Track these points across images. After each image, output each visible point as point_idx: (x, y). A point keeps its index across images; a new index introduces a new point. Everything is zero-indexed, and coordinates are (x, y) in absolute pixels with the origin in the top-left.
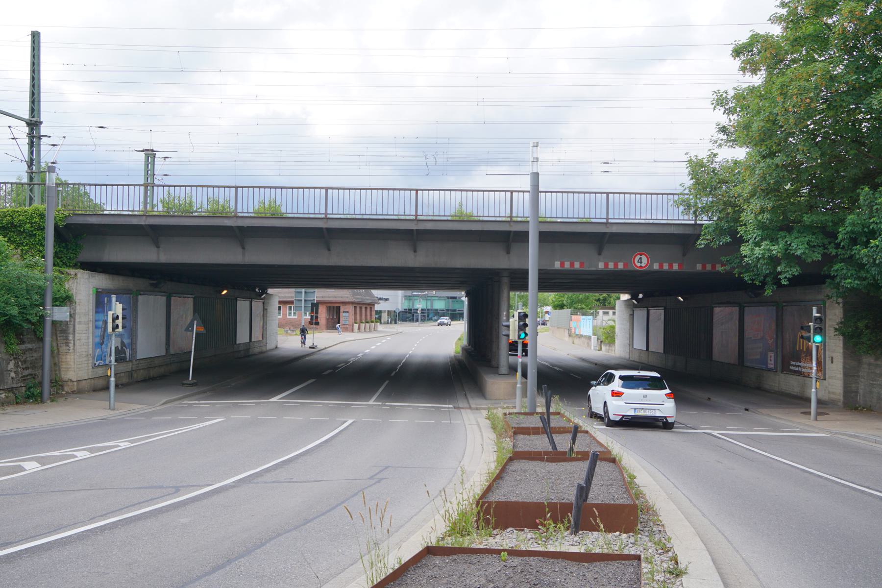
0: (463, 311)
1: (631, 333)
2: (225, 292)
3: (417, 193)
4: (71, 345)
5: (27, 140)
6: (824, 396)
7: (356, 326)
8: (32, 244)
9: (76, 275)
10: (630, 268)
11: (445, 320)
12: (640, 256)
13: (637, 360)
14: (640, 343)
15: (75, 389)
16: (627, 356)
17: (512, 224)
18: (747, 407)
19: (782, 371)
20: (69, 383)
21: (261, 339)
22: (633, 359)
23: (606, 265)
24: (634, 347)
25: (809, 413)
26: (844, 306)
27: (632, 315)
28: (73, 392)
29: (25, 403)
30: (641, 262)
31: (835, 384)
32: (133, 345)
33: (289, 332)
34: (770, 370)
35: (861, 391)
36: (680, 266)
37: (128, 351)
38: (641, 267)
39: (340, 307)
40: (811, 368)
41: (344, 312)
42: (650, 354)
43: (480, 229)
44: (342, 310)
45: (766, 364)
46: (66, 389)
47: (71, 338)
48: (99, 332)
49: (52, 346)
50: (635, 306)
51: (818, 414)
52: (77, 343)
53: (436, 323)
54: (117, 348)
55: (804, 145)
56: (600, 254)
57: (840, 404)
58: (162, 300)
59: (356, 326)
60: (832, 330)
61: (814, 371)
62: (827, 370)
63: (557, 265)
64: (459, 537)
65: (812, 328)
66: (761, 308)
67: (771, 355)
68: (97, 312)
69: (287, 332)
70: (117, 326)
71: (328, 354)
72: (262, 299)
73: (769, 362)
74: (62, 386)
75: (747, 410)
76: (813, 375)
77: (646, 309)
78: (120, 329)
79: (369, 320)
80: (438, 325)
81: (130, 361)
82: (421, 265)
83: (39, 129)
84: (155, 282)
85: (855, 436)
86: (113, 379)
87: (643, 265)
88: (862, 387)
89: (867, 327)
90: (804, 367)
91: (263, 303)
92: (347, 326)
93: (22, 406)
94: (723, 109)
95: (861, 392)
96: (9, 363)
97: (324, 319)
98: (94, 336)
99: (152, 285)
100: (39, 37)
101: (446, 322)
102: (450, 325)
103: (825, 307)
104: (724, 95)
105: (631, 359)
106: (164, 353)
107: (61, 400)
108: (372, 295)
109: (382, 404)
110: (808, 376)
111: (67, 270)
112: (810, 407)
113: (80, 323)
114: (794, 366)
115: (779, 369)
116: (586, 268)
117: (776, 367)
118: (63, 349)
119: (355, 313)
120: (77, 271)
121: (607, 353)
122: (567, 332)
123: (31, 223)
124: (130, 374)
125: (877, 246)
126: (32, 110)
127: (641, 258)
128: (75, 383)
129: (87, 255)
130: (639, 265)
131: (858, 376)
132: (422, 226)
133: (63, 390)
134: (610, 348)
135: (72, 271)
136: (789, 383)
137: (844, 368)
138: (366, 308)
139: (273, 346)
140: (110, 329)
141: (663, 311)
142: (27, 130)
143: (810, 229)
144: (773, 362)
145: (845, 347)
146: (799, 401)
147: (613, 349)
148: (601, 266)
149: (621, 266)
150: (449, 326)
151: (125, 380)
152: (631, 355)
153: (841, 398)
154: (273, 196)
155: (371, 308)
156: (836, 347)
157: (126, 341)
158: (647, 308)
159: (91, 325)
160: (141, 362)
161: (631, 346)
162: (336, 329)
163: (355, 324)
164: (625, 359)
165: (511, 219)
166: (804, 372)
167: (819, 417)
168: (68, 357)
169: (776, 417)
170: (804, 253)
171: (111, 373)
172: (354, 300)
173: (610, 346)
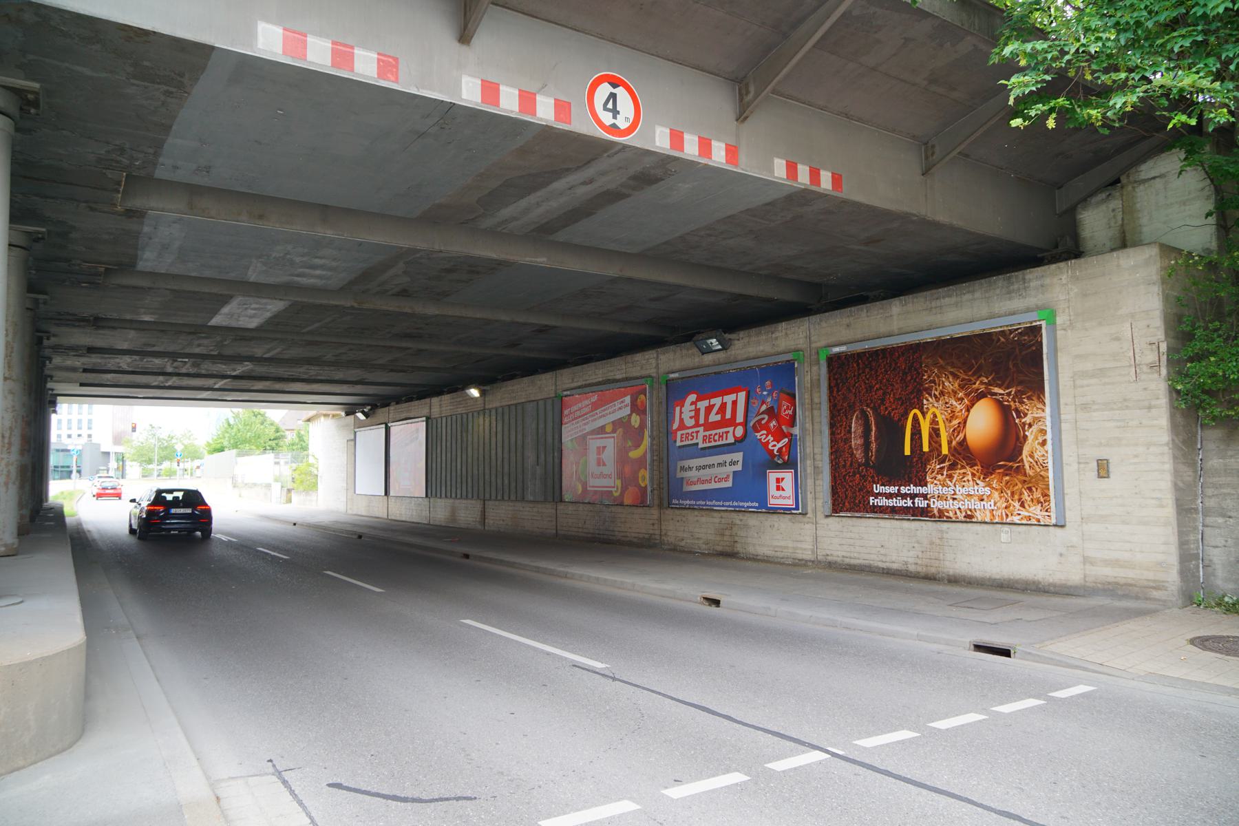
0: (68, 467)
12: (611, 89)
13: (364, 514)
14: (370, 482)
22: (354, 513)
24: (357, 493)
30: (615, 113)
35: (1216, 551)
38: (613, 129)
42: (392, 501)
56: (464, 37)
77: (384, 426)
87: (623, 124)
109: (1031, 323)
116: (406, 83)
122: (230, 482)
127: (613, 96)
130: (607, 118)
152: (349, 507)
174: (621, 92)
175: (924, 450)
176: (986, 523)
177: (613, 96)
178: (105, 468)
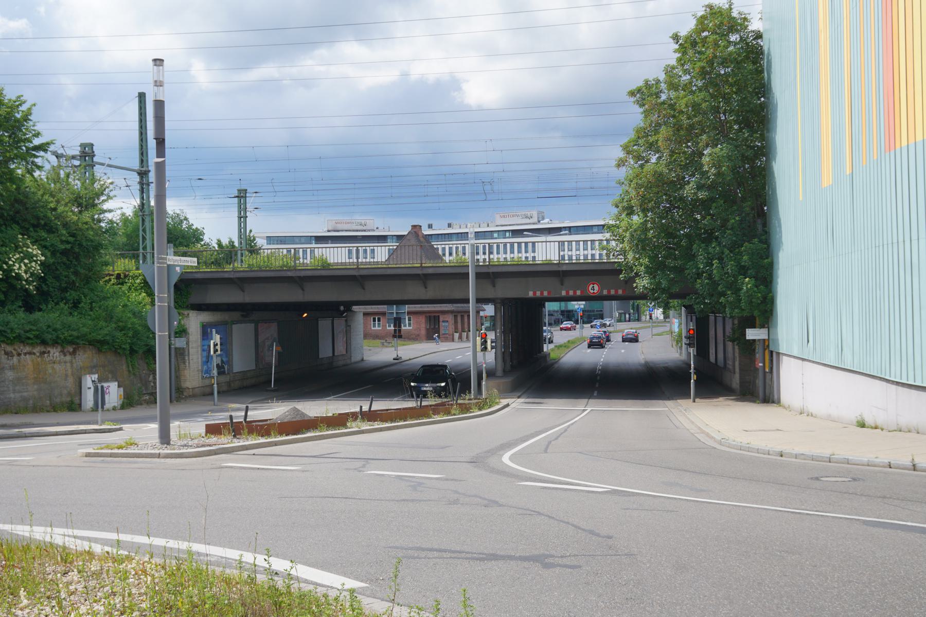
2: (305, 315)
4: (187, 364)
5: (138, 187)
9: (188, 314)
15: (191, 394)
20: (187, 390)
21: (344, 353)
28: (190, 396)
30: (594, 290)
32: (230, 363)
33: (385, 344)
36: (623, 291)
37: (226, 367)
39: (439, 316)
41: (443, 322)
44: (441, 319)
46: (185, 394)
47: (187, 359)
48: (205, 354)
49: (175, 365)
52: (191, 361)
54: (218, 365)
58: (251, 326)
59: (457, 335)
63: (531, 294)
64: (30, 277)
68: (203, 339)
69: (383, 344)
70: (217, 350)
71: (408, 365)
72: (344, 317)
74: (182, 392)
78: (219, 352)
81: (228, 373)
83: (148, 177)
84: (244, 313)
86: (215, 386)
87: (595, 291)
91: (346, 321)
92: (447, 336)
96: (149, 377)
97: (424, 329)
98: (202, 357)
99: (242, 316)
100: (145, 97)
106: (254, 368)
107: (182, 401)
111: (183, 312)
113: (192, 348)
118: (182, 366)
119: (456, 322)
120: (188, 311)
124: (229, 383)
126: (142, 161)
128: (191, 390)
129: (195, 299)
130: (592, 291)
133: (183, 395)
135: (186, 312)
138: (462, 317)
139: (358, 358)
140: (212, 352)
142: (138, 179)
151: (225, 388)
154: (324, 253)
157: (224, 359)
159: (200, 349)
160: (237, 374)
162: (434, 339)
163: (455, 334)
168: (186, 371)
171: (215, 381)
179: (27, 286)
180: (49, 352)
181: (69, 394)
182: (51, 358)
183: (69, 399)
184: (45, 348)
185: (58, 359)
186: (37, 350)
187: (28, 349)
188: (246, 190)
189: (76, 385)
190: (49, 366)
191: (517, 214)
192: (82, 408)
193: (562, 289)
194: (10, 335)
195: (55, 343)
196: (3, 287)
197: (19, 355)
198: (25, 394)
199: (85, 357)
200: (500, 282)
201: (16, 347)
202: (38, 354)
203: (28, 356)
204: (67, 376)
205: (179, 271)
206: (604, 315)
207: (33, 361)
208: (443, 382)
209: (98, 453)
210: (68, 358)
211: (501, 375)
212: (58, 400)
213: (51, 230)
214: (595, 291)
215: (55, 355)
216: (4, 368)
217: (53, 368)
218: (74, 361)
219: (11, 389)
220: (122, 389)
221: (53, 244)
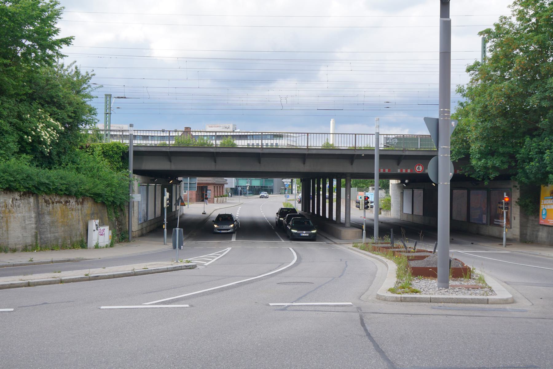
1: (402, 204)
3: (308, 135)
6: (510, 236)
7: (216, 199)
8: (112, 161)
10: (413, 172)
11: (264, 194)
13: (406, 220)
14: (407, 210)
16: (399, 218)
17: (356, 151)
18: (472, 242)
19: (490, 224)
23: (402, 170)
25: (502, 245)
26: (520, 190)
27: (402, 193)
29: (122, 242)
30: (419, 169)
31: (516, 230)
34: (484, 224)
38: (419, 171)
40: (503, 222)
43: (340, 153)
45: (482, 221)
50: (404, 188)
51: (506, 245)
53: (258, 196)
55: (500, 119)
56: (398, 165)
57: (518, 240)
60: (515, 203)
61: (505, 224)
62: (512, 223)
65: (504, 203)
66: (479, 191)
67: (485, 216)
73: (483, 220)
75: (472, 244)
76: (504, 226)
79: (216, 196)
80: (260, 198)
82: (308, 171)
85: (522, 252)
87: (420, 170)
88: (529, 231)
89: (531, 202)
90: (501, 222)
93: (30, 253)
94: (461, 94)
95: (528, 234)
101: (265, 195)
102: (268, 198)
103: (511, 191)
104: (462, 87)
105: (401, 219)
108: (224, 179)
110: (501, 226)
112: (503, 242)
114: (496, 222)
115: (489, 223)
117: (487, 222)
119: (215, 191)
121: (385, 216)
123: (112, 151)
125: (533, 165)
127: (419, 167)
130: (418, 170)
131: (527, 226)
132: (310, 152)
134: (387, 213)
136: (493, 231)
137: (520, 222)
141: (423, 191)
143: (503, 154)
144: (485, 220)
145: (521, 212)
146: (497, 239)
147: (390, 213)
148: (399, 171)
149: (409, 171)
150: (267, 199)
153: (519, 237)
155: (222, 187)
156: (516, 211)
158: (412, 189)
161: (402, 212)
164: (397, 219)
165: (355, 148)
166: (501, 225)
167: (507, 246)
169: (486, 246)
170: (499, 165)
172: (215, 182)
173: (387, 211)
174: (420, 166)
175: (344, 189)
176: (145, 131)
177: (419, 167)
178: (284, 188)
179: (46, 150)
180: (70, 201)
181: (81, 235)
182: (71, 206)
183: (81, 239)
184: (68, 198)
185: (74, 207)
186: (63, 200)
187: (57, 199)
188: (111, 95)
189: (84, 228)
190: (70, 212)
191: (220, 125)
192: (88, 246)
193: (398, 168)
194: (51, 187)
195: (76, 196)
196: (29, 149)
197: (53, 203)
198: (56, 234)
199: (88, 206)
200: (356, 162)
201: (51, 197)
202: (64, 203)
203: (58, 204)
204: (79, 221)
205: (454, 126)
206: (274, 190)
207: (61, 208)
208: (315, 230)
209: (415, 298)
210: (80, 206)
211: (349, 226)
212: (74, 239)
213: (60, 107)
214: (420, 170)
215: (73, 203)
216: (44, 213)
217: (72, 215)
218: (83, 209)
219: (48, 230)
220: (111, 231)
221: (63, 118)
